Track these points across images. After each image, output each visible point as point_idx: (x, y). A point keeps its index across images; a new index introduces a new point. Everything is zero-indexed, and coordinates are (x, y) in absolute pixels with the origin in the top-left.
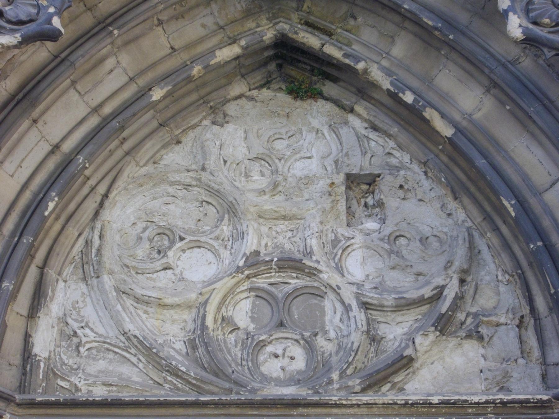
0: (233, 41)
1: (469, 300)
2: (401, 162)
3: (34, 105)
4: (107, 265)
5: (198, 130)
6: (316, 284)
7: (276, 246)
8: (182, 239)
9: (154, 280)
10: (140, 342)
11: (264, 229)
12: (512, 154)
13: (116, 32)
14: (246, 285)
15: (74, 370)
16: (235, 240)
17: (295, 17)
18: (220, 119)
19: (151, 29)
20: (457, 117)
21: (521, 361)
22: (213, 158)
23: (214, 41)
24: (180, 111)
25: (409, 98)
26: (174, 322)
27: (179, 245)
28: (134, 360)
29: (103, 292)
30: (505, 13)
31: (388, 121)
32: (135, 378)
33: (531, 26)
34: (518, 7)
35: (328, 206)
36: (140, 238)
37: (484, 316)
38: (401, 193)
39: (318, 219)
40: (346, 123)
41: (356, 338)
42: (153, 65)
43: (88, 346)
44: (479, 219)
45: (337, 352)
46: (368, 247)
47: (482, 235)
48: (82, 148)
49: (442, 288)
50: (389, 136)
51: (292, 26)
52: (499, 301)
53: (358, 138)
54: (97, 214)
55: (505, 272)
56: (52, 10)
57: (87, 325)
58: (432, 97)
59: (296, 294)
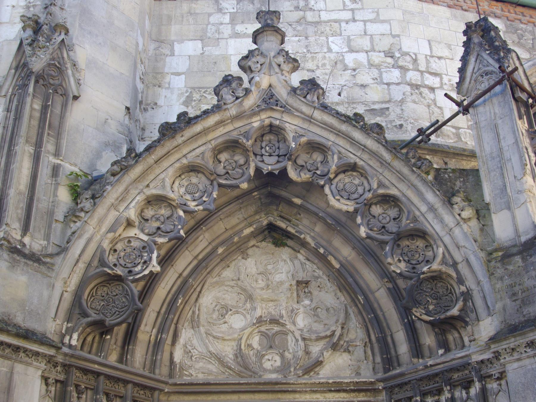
0: (251, 225)
1: (345, 335)
2: (319, 275)
3: (172, 261)
4: (202, 323)
5: (236, 261)
6: (284, 330)
7: (269, 313)
8: (231, 310)
9: (220, 328)
10: (216, 355)
11: (264, 305)
12: (363, 276)
13: (204, 228)
14: (256, 331)
15: (190, 367)
16: (252, 310)
17: (275, 213)
19: (217, 223)
20: (341, 259)
21: (365, 362)
22: (243, 274)
23: (242, 225)
24: (229, 254)
25: (322, 251)
27: (230, 313)
28: (213, 362)
31: (313, 257)
32: (215, 370)
33: (369, 232)
34: (364, 223)
35: (289, 296)
36: (214, 310)
37: (351, 342)
38: (319, 289)
39: (285, 302)
41: (300, 353)
42: (218, 237)
43: (195, 357)
44: (350, 301)
45: (293, 359)
46: (305, 313)
47: (351, 307)
48: (165, 155)
50: (314, 263)
51: (274, 218)
52: (357, 336)
53: (301, 264)
54: (197, 300)
55: (359, 323)
56: (180, 227)
57: (195, 348)
59: (277, 333)
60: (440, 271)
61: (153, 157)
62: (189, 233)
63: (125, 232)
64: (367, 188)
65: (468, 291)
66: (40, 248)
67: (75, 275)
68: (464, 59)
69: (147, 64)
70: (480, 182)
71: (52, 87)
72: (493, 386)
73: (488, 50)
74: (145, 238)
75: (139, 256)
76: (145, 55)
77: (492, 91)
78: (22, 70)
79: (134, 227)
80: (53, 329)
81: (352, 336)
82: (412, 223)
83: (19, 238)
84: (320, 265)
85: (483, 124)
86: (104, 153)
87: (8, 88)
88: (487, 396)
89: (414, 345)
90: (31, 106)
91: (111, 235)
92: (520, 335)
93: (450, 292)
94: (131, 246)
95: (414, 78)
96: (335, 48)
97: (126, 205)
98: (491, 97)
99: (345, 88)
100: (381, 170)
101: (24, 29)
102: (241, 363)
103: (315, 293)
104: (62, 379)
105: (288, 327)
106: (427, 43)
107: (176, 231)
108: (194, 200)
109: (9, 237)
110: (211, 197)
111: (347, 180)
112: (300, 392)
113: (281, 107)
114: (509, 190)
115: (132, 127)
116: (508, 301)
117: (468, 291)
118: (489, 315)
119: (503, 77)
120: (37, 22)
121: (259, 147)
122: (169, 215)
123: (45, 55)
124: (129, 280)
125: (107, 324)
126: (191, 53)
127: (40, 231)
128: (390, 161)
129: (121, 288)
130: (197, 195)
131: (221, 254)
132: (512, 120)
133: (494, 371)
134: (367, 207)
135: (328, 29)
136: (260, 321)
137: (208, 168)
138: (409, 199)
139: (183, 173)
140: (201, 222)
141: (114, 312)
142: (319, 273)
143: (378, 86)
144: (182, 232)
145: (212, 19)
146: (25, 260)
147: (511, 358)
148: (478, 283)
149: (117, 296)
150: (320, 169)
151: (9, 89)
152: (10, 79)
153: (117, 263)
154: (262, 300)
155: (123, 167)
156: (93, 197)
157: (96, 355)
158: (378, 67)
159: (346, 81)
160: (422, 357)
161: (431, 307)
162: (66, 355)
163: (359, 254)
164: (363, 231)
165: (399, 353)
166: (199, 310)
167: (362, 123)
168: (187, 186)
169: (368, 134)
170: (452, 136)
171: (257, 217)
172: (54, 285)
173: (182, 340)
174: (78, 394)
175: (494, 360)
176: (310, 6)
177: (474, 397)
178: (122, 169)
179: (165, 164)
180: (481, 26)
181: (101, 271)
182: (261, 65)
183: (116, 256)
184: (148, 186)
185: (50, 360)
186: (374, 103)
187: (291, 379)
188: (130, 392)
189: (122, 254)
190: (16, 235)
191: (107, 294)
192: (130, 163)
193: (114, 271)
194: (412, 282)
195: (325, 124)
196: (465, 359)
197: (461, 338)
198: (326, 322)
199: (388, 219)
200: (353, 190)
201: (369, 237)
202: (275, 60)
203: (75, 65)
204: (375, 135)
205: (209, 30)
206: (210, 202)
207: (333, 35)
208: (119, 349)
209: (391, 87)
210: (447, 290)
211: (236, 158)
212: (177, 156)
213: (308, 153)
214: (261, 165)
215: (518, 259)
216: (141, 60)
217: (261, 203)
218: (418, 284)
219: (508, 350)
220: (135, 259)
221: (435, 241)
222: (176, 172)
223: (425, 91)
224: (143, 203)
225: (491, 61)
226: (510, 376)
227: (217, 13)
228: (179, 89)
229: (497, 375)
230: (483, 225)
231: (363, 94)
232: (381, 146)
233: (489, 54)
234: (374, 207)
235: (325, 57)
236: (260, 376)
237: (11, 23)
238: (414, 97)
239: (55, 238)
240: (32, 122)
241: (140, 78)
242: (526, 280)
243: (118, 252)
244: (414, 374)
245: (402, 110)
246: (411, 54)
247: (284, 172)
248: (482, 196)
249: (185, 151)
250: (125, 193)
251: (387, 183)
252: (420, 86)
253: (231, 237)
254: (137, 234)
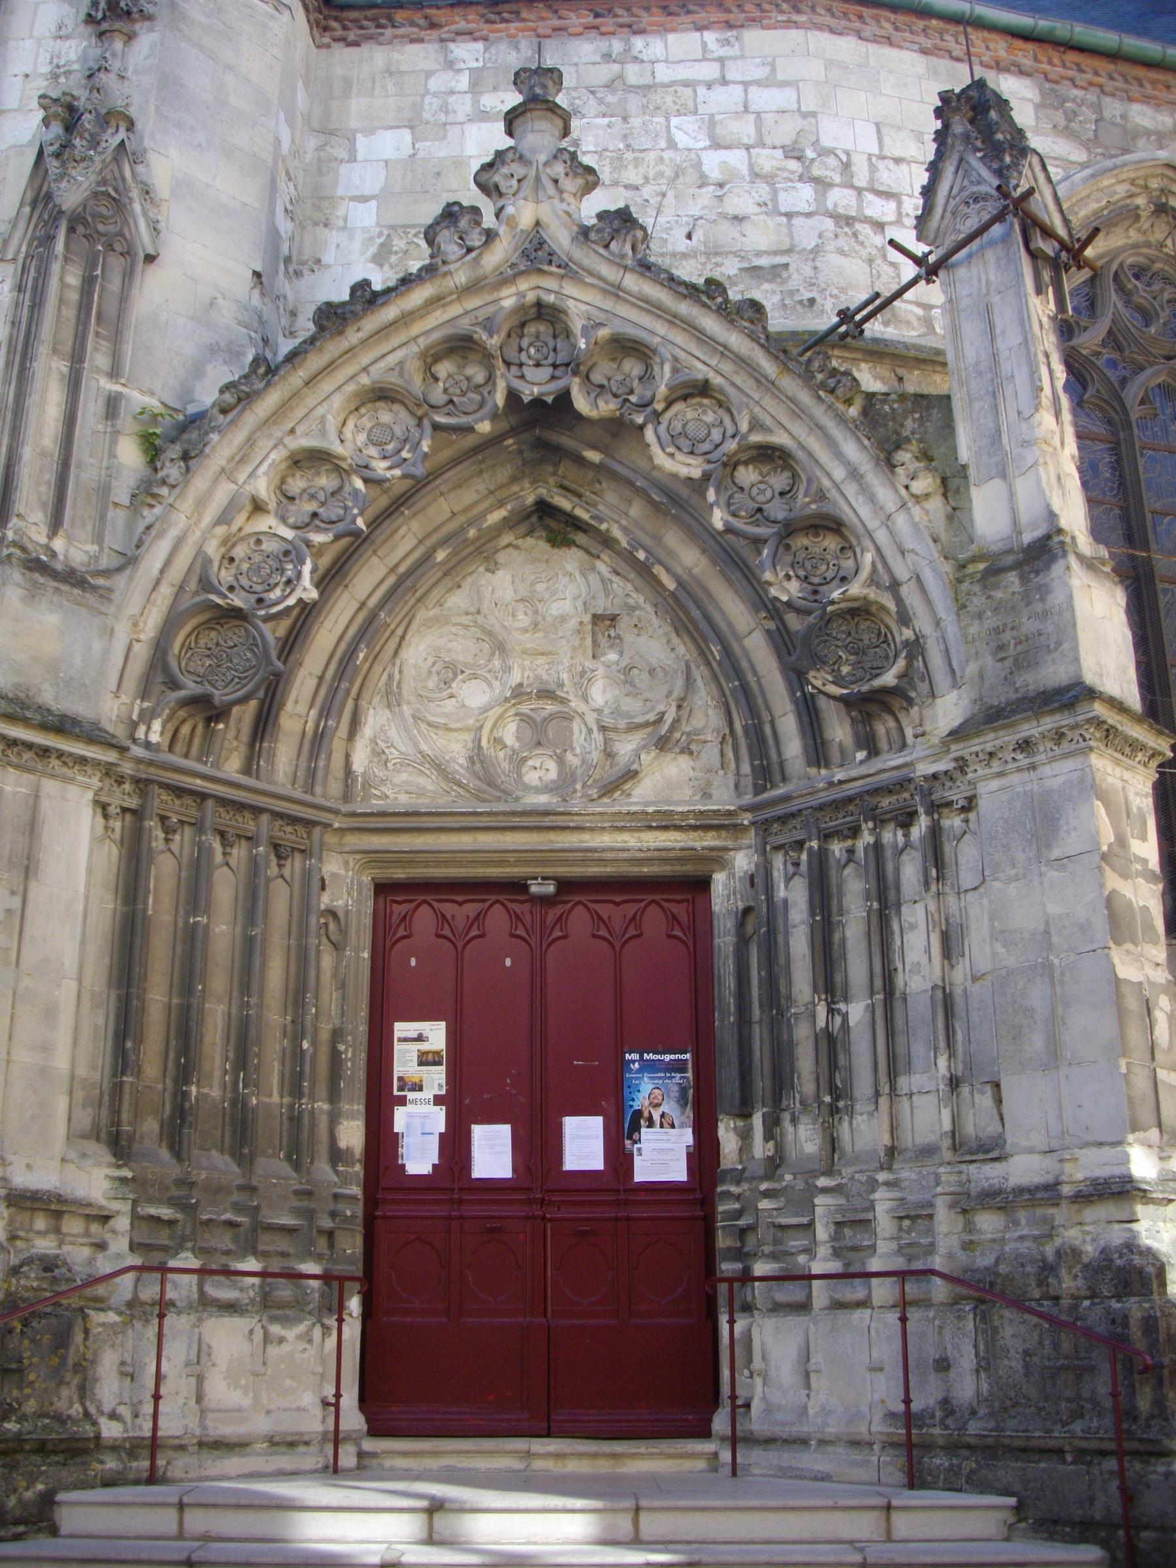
0: (501, 504)
1: (684, 721)
3: (344, 578)
11: (527, 663)
15: (384, 781)
17: (552, 480)
18: (492, 567)
20: (680, 571)
21: (721, 772)
25: (641, 555)
26: (457, 741)
27: (460, 677)
29: (404, 719)
30: (711, 506)
32: (430, 787)
33: (730, 519)
35: (577, 643)
40: (593, 569)
41: (596, 756)
47: (698, 667)
49: (663, 714)
54: (396, 652)
56: (355, 511)
58: (662, 555)
59: (552, 717)
60: (865, 598)
62: (375, 523)
64: (730, 432)
65: (917, 639)
66: (86, 559)
67: (155, 610)
68: (934, 168)
69: (300, 181)
70: (952, 420)
71: (103, 239)
72: (952, 822)
73: (979, 150)
74: (288, 534)
76: (296, 163)
77: (985, 235)
78: (45, 207)
79: (267, 512)
80: (115, 712)
81: (697, 722)
82: (815, 502)
83: (43, 540)
84: (639, 582)
85: (964, 303)
86: (209, 368)
87: (19, 244)
88: (941, 843)
89: (811, 742)
90: (61, 279)
91: (221, 530)
92: (1004, 727)
93: (884, 639)
95: (842, 203)
96: (682, 139)
97: (250, 469)
98: (982, 248)
99: (700, 222)
100: (756, 396)
101: (46, 122)
102: (481, 774)
103: (629, 638)
104: (133, 806)
105: (573, 704)
106: (873, 129)
107: (348, 519)
108: (385, 458)
109: (25, 540)
111: (690, 414)
112: (591, 829)
113: (559, 267)
114: (1005, 440)
115: (268, 311)
116: (989, 660)
117: (917, 639)
118: (955, 685)
119: (1006, 207)
120: (71, 109)
121: (516, 348)
123: (86, 175)
125: (216, 702)
126: (390, 154)
127: (84, 526)
128: (773, 376)
130: (390, 447)
131: (442, 563)
132: (1021, 297)
133: (957, 795)
134: (729, 469)
135: (669, 99)
136: (518, 693)
138: (810, 454)
139: (363, 404)
142: (638, 598)
143: (769, 220)
144: (360, 523)
145: (434, 84)
146: (56, 584)
147: (988, 771)
148: (938, 623)
150: (637, 391)
151: (20, 246)
152: (22, 226)
153: (235, 584)
154: (524, 652)
155: (242, 395)
156: (186, 457)
157: (199, 760)
158: (769, 179)
159: (703, 208)
160: (827, 766)
161: (845, 670)
162: (138, 761)
163: (715, 564)
164: (718, 519)
165: (784, 757)
166: (400, 672)
167: (720, 300)
168: (370, 430)
169: (732, 322)
170: (916, 323)
171: (515, 488)
172: (112, 631)
173: (367, 731)
174: (167, 833)
175: (957, 775)
176: (635, 53)
177: (917, 844)
178: (240, 400)
179: (327, 386)
180: (970, 98)
181: (203, 601)
182: (519, 181)
183: (233, 571)
184: (292, 431)
185: (108, 770)
186: (759, 254)
187: (574, 805)
188: (264, 828)
189: (245, 566)
190: (38, 535)
191: (218, 644)
192: (255, 387)
194: (811, 619)
195: (647, 301)
196: (904, 771)
197: (901, 730)
198: (649, 695)
199: (769, 494)
200: (702, 434)
201: (729, 530)
202: (548, 170)
203: (147, 193)
204: (746, 324)
205: (426, 107)
207: (679, 113)
208: (243, 748)
209: (795, 221)
210: (879, 635)
211: (469, 371)
212: (349, 370)
213: (613, 360)
214: (518, 384)
215: (1012, 577)
216: (288, 174)
217: (523, 459)
218: (823, 623)
219: (982, 756)
220: (270, 575)
221: (857, 537)
222: (348, 401)
223: (865, 230)
224: (284, 465)
225: (985, 173)
226: (983, 803)
227: (444, 69)
228: (365, 230)
229: (961, 803)
230: (954, 509)
231: (737, 235)
232: (756, 347)
233: (981, 158)
234: (741, 469)
235: (661, 160)
236: (517, 799)
237: (22, 110)
238: (842, 242)
239: (115, 538)
240: (64, 312)
241: (286, 210)
242: (1024, 620)
244: (809, 798)
245: (815, 268)
246: (839, 152)
247: (564, 398)
248: (954, 449)
249: (365, 359)
251: (769, 421)
252: (854, 219)
253: (462, 529)
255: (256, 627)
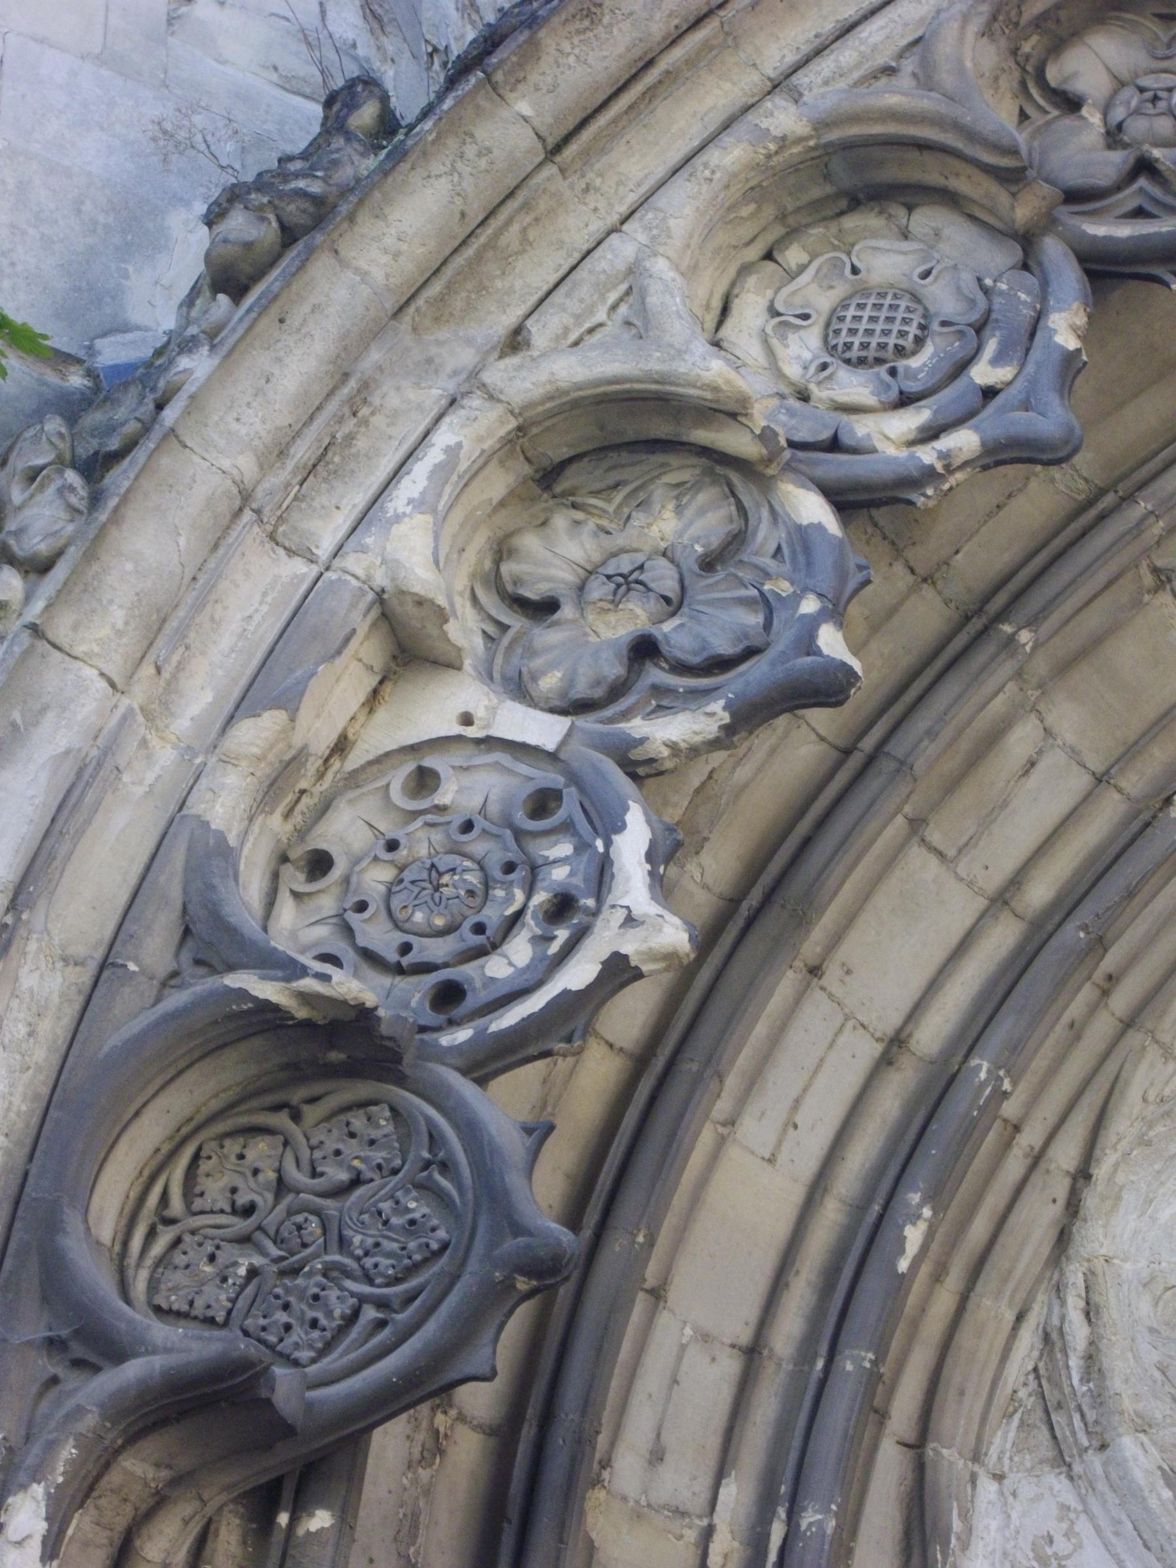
3: (802, 920)
4: (1127, 1404)
13: (1025, 636)
19: (1137, 604)
54: (1063, 1239)
56: (809, 605)
61: (524, 107)
63: (381, 714)
75: (509, 868)
79: (452, 665)
94: (441, 809)
97: (358, 498)
108: (905, 401)
110: (1036, 354)
122: (715, 542)
124: (442, 1055)
129: (385, 1125)
137: (971, 136)
139: (792, 234)
140: (1001, 599)
141: (340, 1310)
149: (360, 1191)
153: (340, 947)
155: (293, 210)
166: (1090, 1313)
168: (835, 316)
178: (289, 235)
183: (327, 904)
189: (376, 879)
191: (281, 1187)
192: (345, 174)
193: (308, 984)
206: (1033, 381)
222: (728, 215)
243: (336, 873)
250: (332, 406)
254: (479, 713)
255: (436, 1096)
